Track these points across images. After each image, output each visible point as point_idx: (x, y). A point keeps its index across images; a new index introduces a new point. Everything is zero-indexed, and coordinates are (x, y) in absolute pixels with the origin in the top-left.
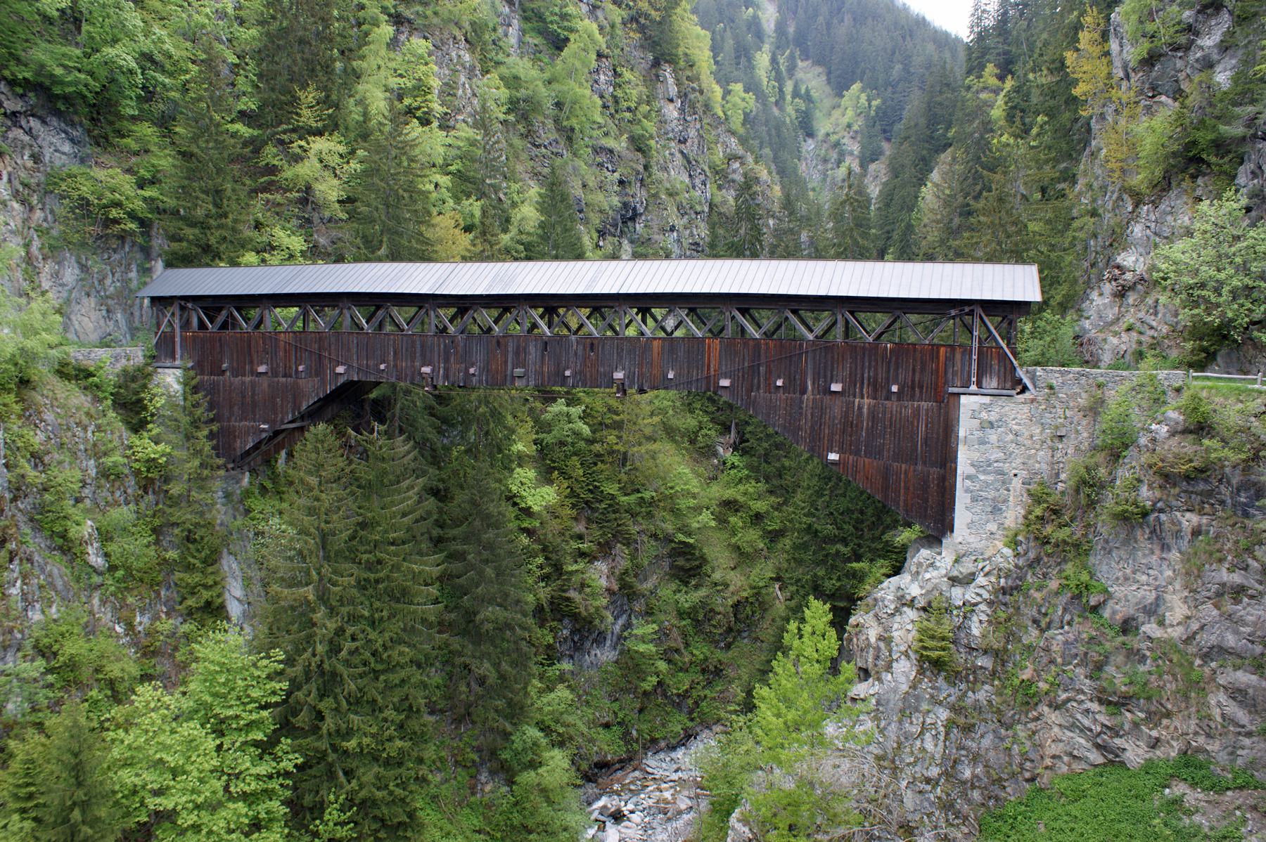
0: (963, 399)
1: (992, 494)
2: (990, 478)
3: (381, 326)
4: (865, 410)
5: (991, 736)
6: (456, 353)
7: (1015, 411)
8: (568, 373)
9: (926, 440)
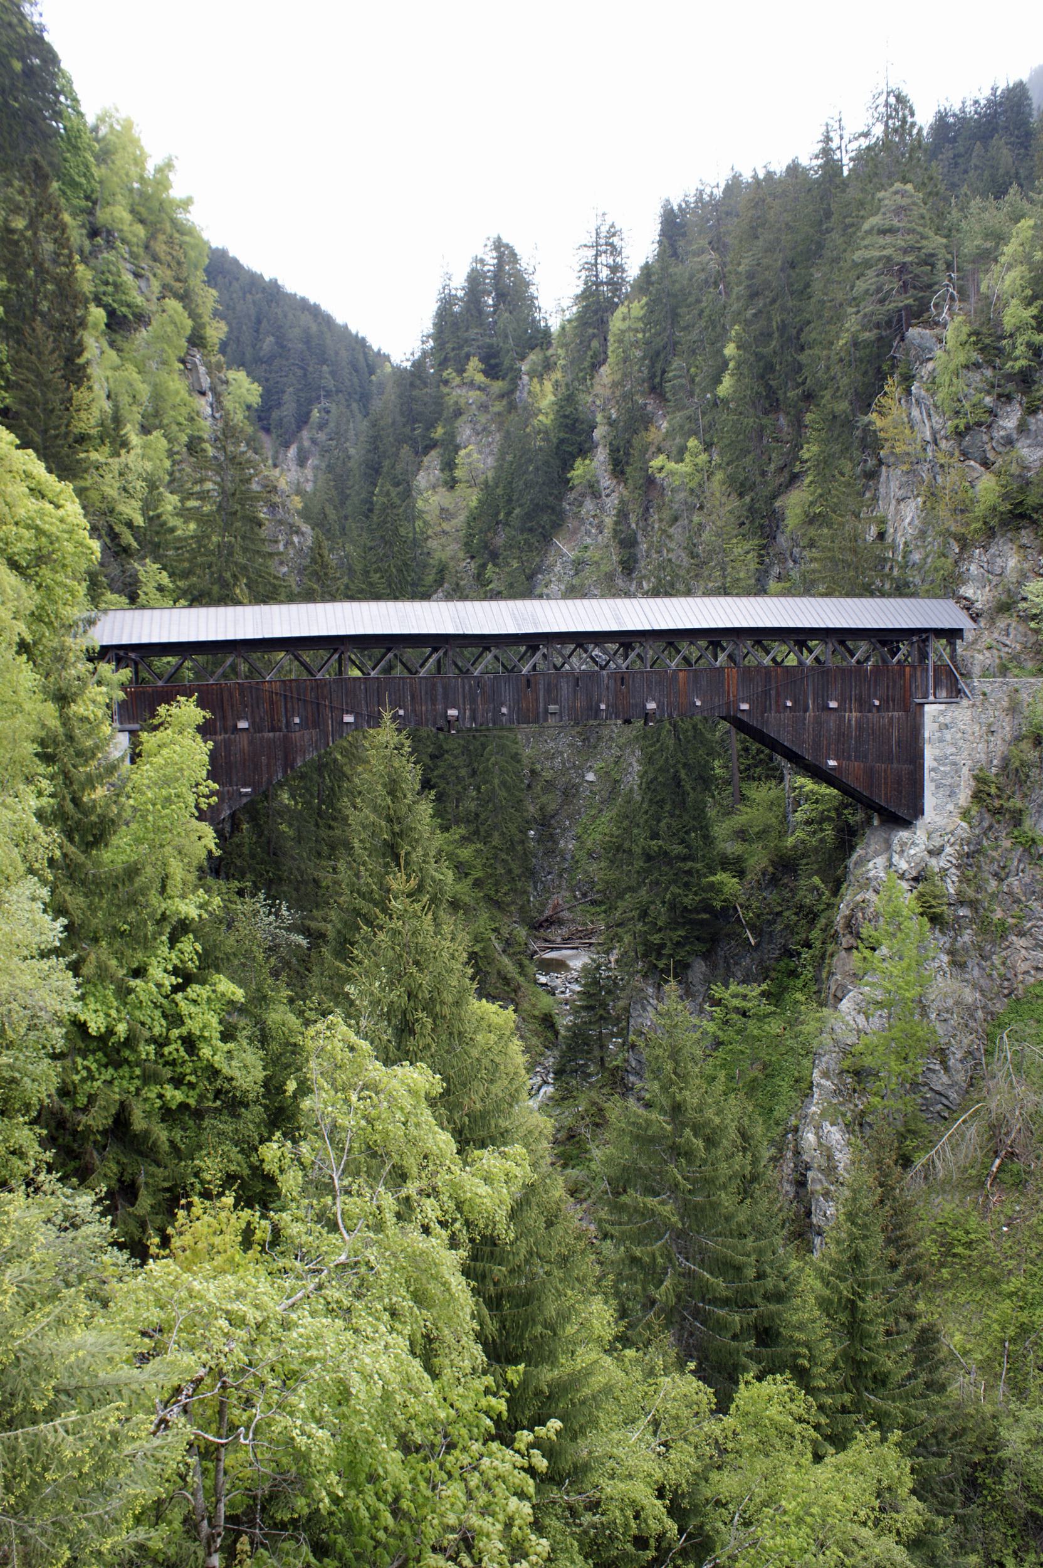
1: (950, 781)
2: (947, 769)
3: (389, 669)
5: (976, 969)
6: (483, 693)
7: (962, 714)
9: (899, 743)
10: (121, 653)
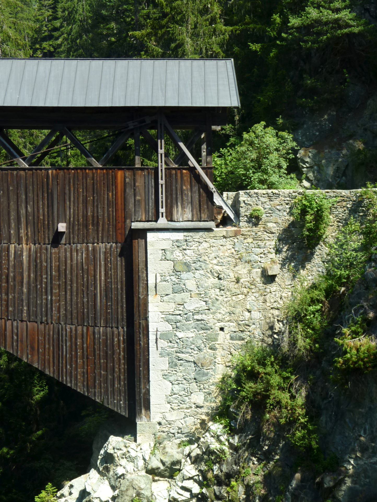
0: (150, 236)
4: (25, 258)
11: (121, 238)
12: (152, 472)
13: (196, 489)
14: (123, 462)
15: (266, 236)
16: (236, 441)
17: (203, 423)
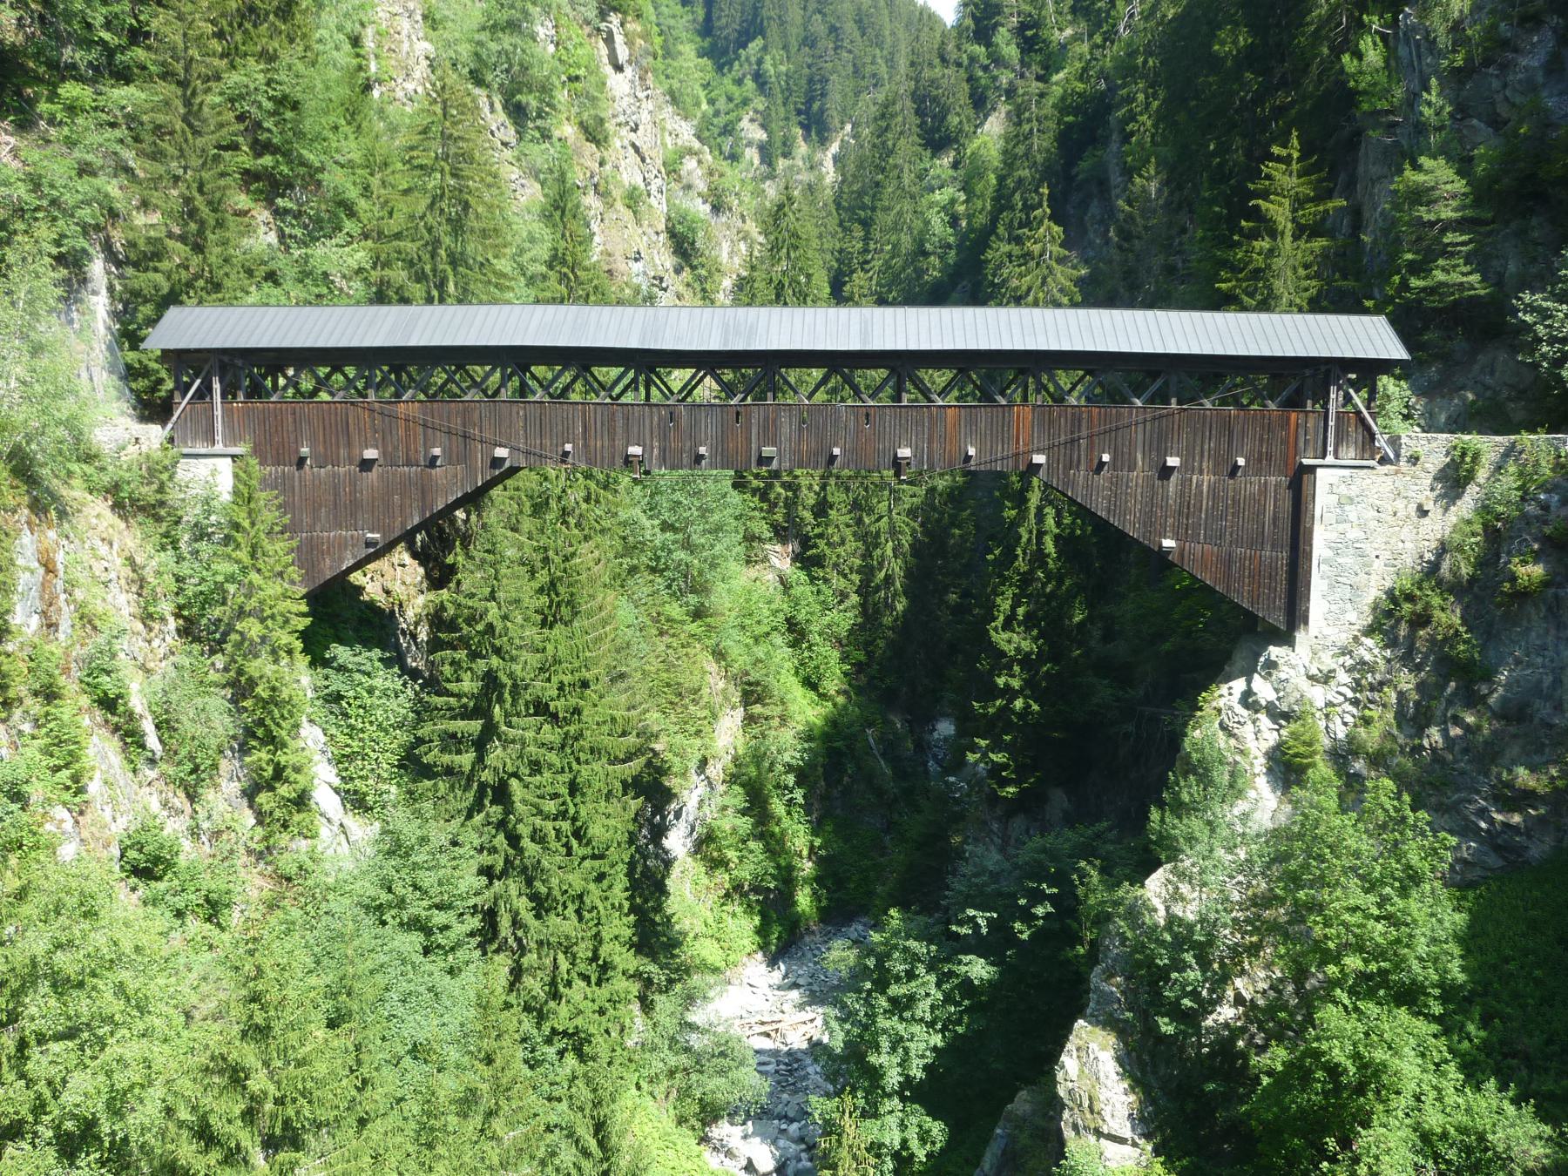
7: (1377, 483)
8: (836, 451)
10: (226, 359)
11: (1291, 473)
12: (1311, 678)
13: (1350, 694)
14: (1285, 668)
15: (1423, 475)
16: (1388, 653)
17: (1355, 638)
